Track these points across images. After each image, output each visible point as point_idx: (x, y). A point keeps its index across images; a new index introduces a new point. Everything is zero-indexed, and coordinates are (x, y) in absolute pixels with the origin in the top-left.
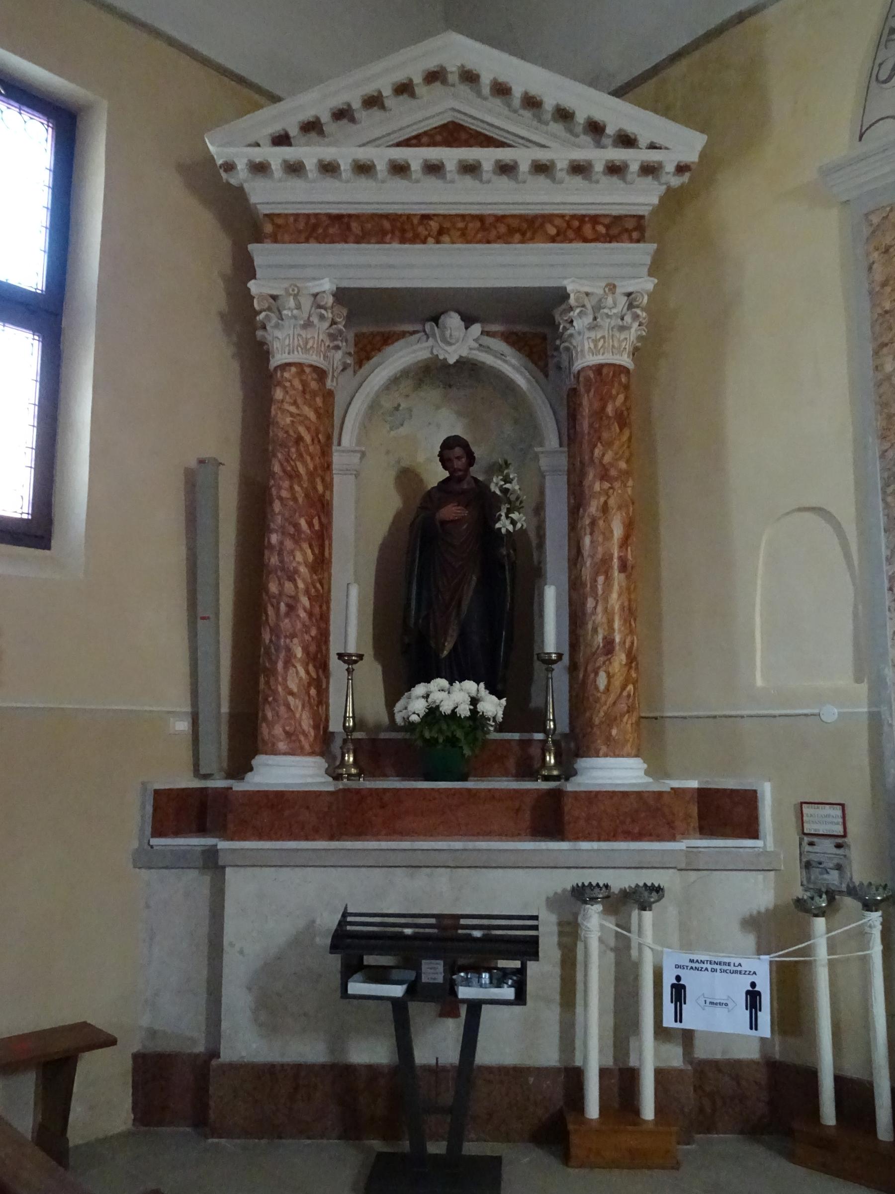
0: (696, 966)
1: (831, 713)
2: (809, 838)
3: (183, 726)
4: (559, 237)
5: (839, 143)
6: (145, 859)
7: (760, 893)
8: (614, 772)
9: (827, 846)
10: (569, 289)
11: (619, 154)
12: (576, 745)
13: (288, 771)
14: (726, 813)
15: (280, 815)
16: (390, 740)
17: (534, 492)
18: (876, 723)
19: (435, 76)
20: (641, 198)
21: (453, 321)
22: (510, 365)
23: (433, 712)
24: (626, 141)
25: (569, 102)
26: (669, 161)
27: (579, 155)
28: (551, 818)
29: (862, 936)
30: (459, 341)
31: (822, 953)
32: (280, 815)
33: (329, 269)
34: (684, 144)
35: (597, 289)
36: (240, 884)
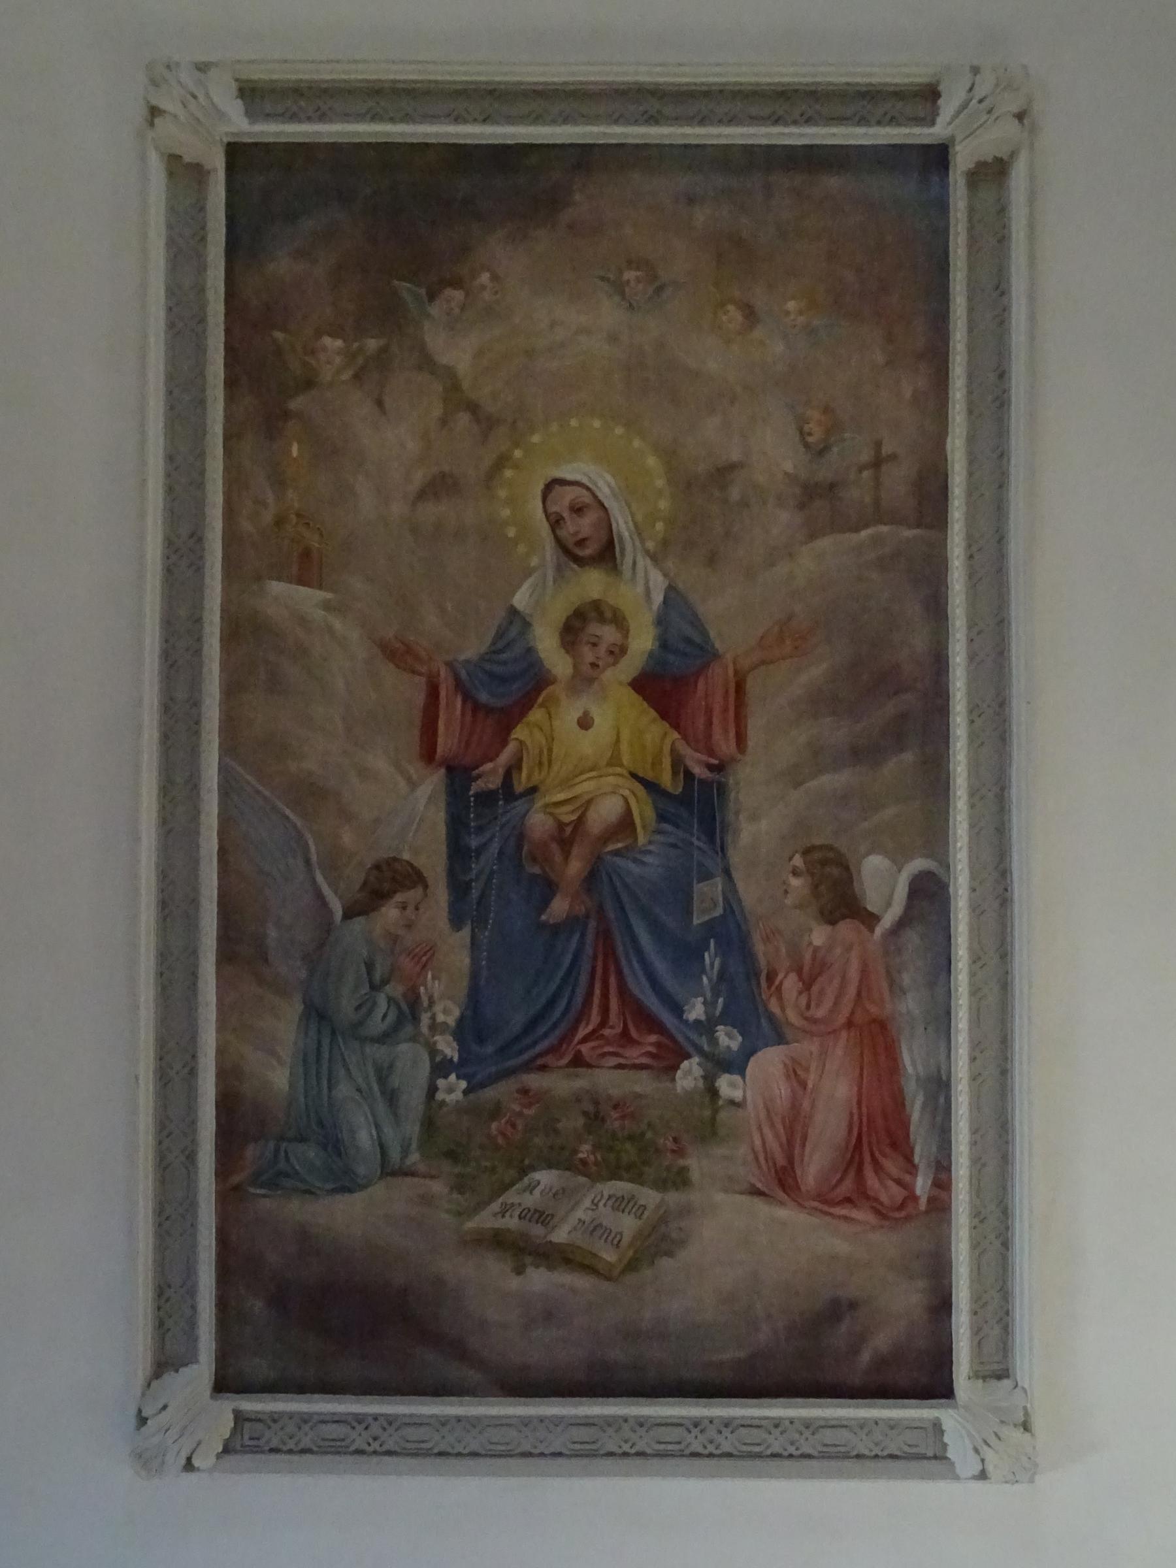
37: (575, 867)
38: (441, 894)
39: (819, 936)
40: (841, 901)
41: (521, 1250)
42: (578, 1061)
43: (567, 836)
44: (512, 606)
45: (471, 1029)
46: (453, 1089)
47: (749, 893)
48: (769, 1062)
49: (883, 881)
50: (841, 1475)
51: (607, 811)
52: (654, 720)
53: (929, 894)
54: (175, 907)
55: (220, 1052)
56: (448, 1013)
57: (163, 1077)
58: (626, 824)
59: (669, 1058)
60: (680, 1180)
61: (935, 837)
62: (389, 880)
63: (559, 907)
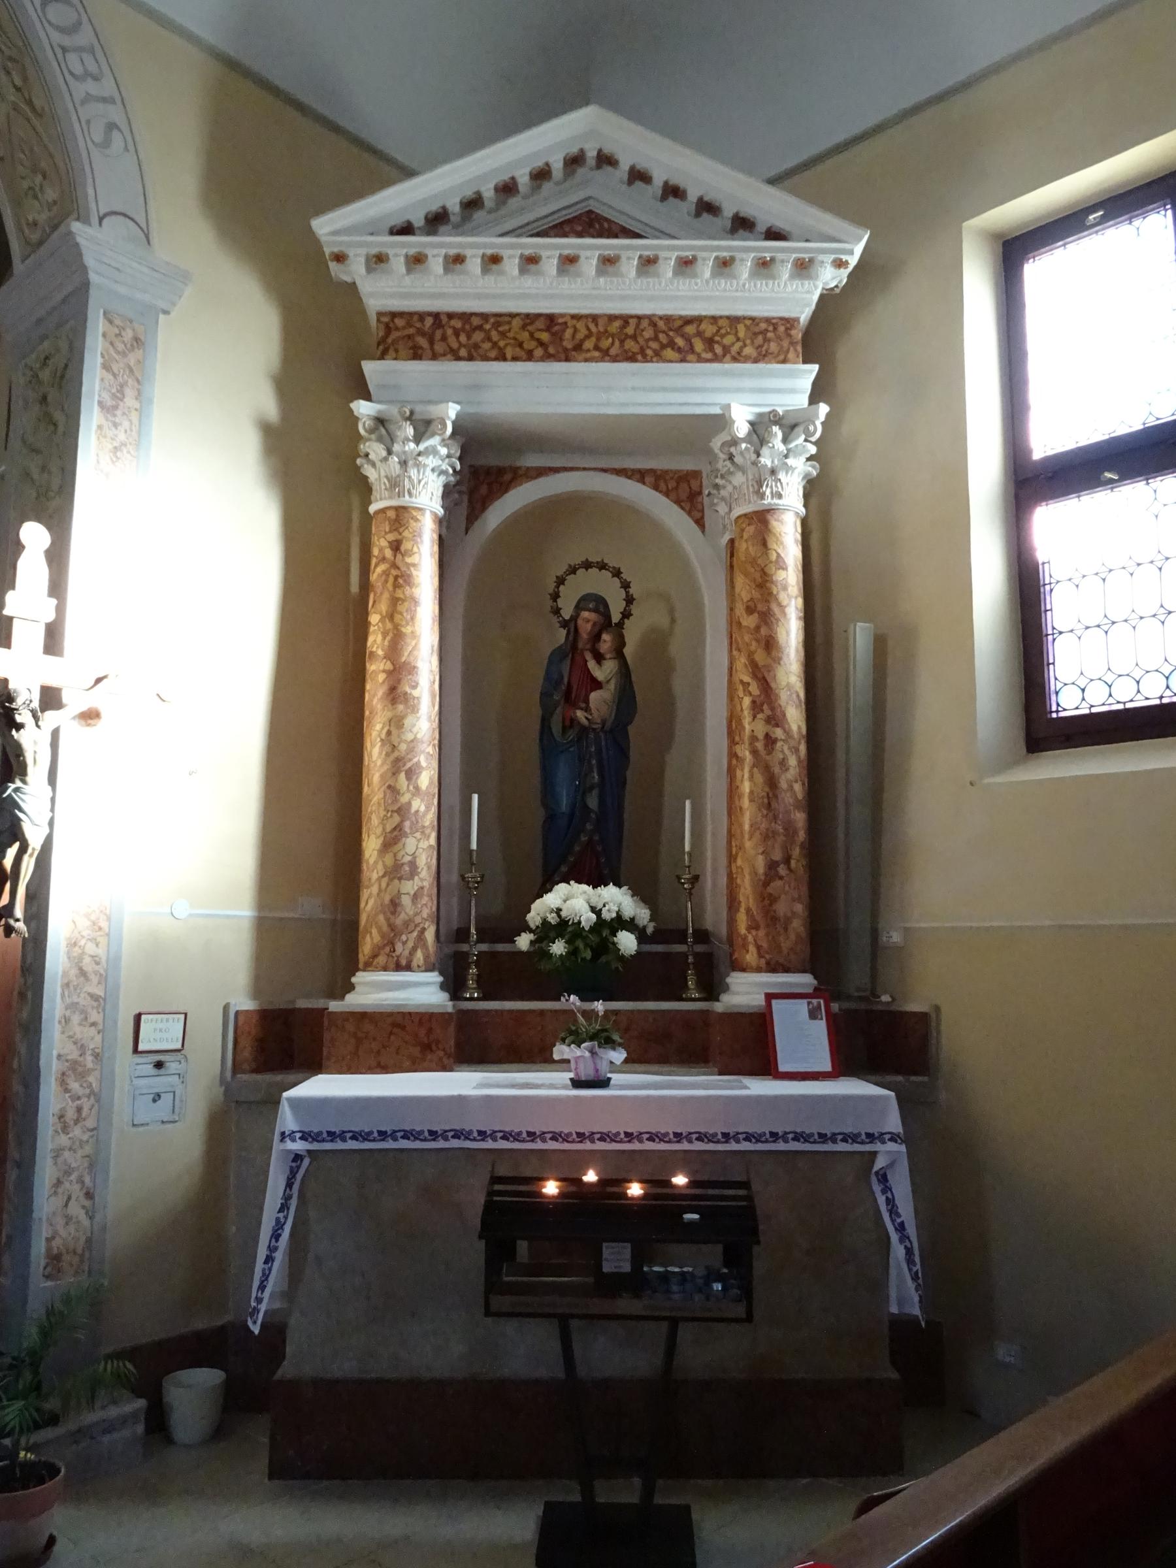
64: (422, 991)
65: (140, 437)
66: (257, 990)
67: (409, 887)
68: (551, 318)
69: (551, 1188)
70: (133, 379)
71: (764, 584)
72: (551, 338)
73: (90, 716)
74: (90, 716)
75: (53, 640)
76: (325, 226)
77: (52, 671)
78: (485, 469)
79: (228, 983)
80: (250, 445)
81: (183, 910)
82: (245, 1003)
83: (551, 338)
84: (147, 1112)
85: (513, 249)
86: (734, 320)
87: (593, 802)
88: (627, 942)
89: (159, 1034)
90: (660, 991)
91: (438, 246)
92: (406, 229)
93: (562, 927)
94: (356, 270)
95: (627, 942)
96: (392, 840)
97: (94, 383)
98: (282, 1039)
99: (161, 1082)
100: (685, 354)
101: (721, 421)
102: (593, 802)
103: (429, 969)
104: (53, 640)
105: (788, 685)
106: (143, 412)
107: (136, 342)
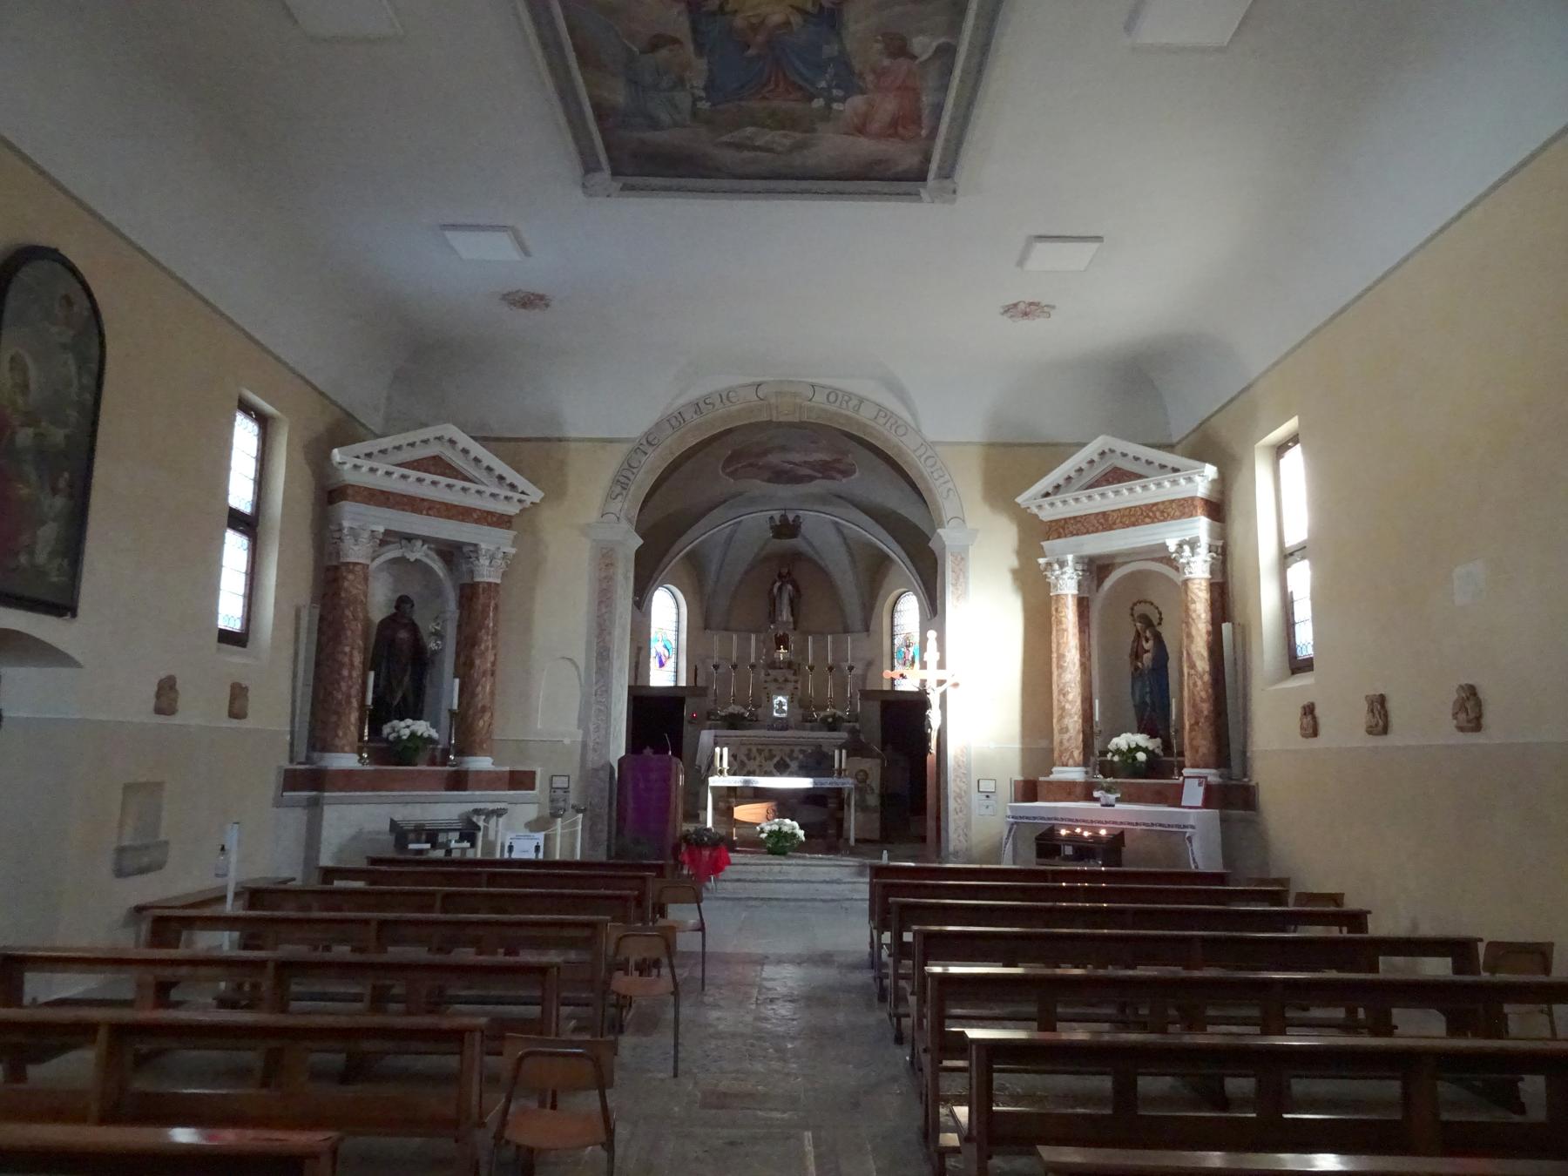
0: (518, 838)
1: (567, 741)
2: (553, 789)
3: (288, 738)
4: (477, 521)
5: (594, 515)
6: (278, 803)
7: (531, 812)
8: (481, 763)
9: (560, 792)
10: (483, 546)
11: (510, 494)
12: (464, 749)
13: (347, 761)
14: (520, 780)
15: (348, 780)
16: (924, 797)
17: (439, 627)
18: (584, 745)
19: (439, 439)
20: (512, 509)
21: (419, 543)
22: (438, 566)
23: (413, 734)
24: (512, 487)
25: (493, 465)
26: (528, 500)
27: (496, 491)
28: (458, 781)
29: (574, 824)
30: (418, 553)
31: (559, 831)
32: (348, 780)
33: (382, 520)
34: (535, 495)
35: (492, 548)
36: (330, 814)
37: (760, 38)
38: (690, 47)
39: (886, 62)
40: (899, 48)
41: (739, 146)
42: (764, 98)
43: (755, 28)
44: (231, 509)
45: (710, 87)
46: (704, 105)
47: (850, 45)
48: (857, 101)
49: (923, 45)
50: (871, 194)
51: (777, 18)
52: (1415, 926)
53: (947, 53)
54: (550, 45)
55: (591, 97)
56: (699, 82)
57: (563, 98)
58: (787, 23)
59: (811, 98)
60: (814, 130)
61: (955, 28)
62: (657, 43)
63: (752, 52)
64: (1075, 774)
65: (965, 592)
66: (1023, 774)
67: (1066, 736)
68: (1104, 514)
69: (1063, 832)
70: (962, 571)
71: (429, 873)
72: (1105, 521)
73: (956, 685)
74: (956, 685)
75: (941, 665)
76: (1019, 500)
77: (941, 675)
78: (1096, 569)
79: (1012, 769)
80: (1007, 580)
81: (992, 746)
82: (1019, 778)
83: (1105, 521)
84: (984, 811)
85: (1082, 495)
86: (1172, 501)
87: (1148, 700)
88: (1141, 756)
89: (987, 786)
90: (1153, 775)
91: (1057, 499)
92: (1047, 495)
93: (1118, 751)
94: (1035, 510)
95: (1141, 756)
96: (1061, 717)
97: (949, 577)
98: (1029, 790)
99: (988, 802)
100: (1154, 520)
101: (1164, 547)
102: (1148, 700)
103: (1077, 765)
104: (941, 665)
105: (1199, 653)
106: (966, 583)
107: (962, 559)
